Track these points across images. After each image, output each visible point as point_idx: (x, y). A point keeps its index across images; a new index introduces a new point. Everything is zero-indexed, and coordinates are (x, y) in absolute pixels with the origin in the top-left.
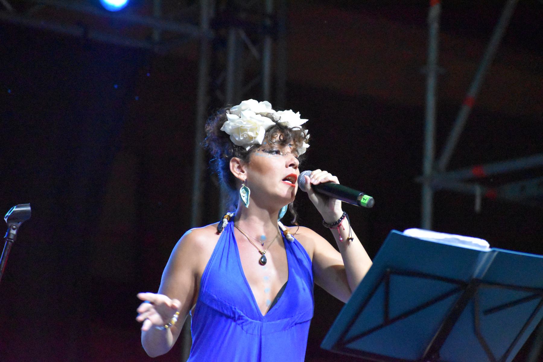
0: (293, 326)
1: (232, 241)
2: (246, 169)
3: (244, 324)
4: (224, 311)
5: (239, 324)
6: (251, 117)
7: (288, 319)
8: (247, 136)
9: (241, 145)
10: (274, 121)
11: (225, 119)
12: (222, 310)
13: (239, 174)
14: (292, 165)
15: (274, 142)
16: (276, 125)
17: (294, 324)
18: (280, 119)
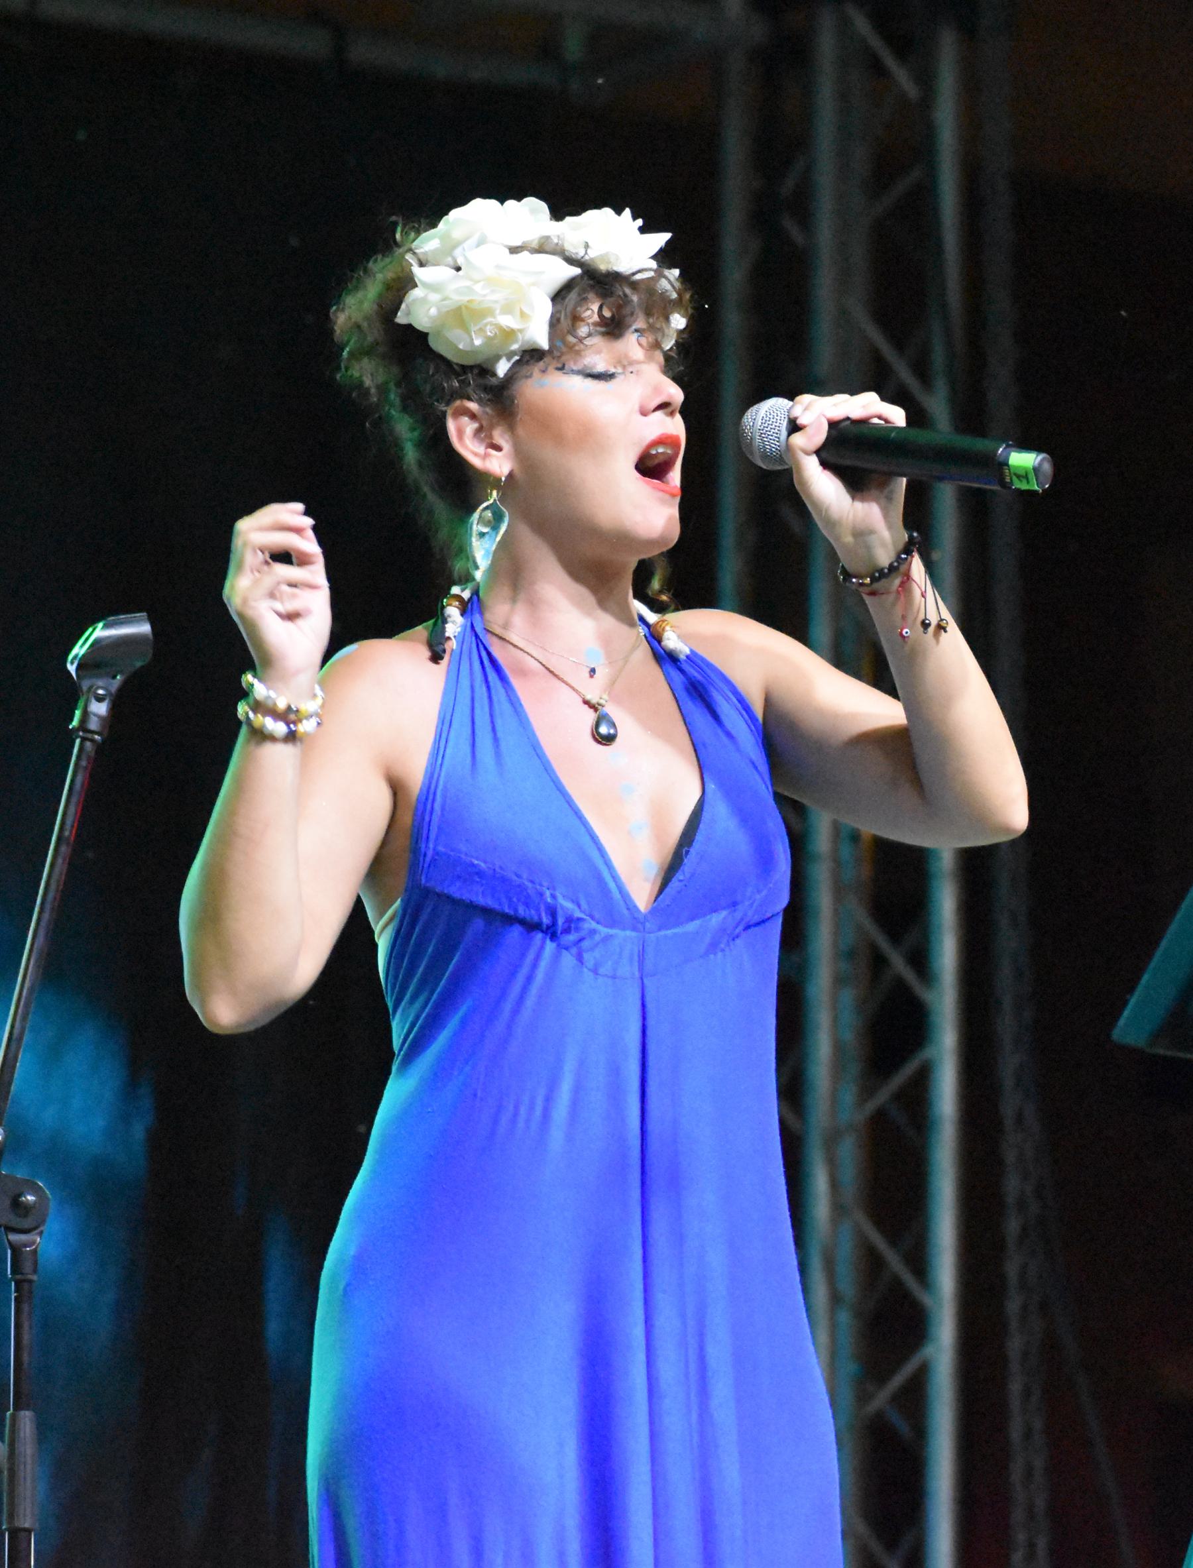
0: (737, 936)
1: (492, 675)
2: (507, 437)
3: (585, 944)
4: (516, 910)
5: (567, 949)
6: (498, 267)
7: (724, 913)
8: (495, 330)
9: (479, 359)
10: (571, 261)
11: (406, 283)
12: (509, 907)
13: (485, 456)
14: (663, 406)
15: (584, 335)
16: (581, 276)
17: (741, 928)
18: (586, 253)
